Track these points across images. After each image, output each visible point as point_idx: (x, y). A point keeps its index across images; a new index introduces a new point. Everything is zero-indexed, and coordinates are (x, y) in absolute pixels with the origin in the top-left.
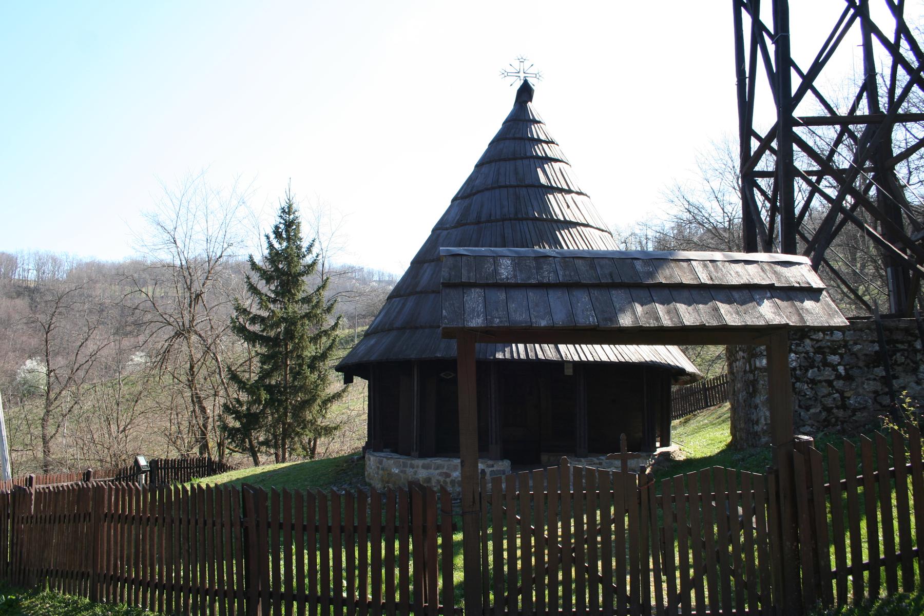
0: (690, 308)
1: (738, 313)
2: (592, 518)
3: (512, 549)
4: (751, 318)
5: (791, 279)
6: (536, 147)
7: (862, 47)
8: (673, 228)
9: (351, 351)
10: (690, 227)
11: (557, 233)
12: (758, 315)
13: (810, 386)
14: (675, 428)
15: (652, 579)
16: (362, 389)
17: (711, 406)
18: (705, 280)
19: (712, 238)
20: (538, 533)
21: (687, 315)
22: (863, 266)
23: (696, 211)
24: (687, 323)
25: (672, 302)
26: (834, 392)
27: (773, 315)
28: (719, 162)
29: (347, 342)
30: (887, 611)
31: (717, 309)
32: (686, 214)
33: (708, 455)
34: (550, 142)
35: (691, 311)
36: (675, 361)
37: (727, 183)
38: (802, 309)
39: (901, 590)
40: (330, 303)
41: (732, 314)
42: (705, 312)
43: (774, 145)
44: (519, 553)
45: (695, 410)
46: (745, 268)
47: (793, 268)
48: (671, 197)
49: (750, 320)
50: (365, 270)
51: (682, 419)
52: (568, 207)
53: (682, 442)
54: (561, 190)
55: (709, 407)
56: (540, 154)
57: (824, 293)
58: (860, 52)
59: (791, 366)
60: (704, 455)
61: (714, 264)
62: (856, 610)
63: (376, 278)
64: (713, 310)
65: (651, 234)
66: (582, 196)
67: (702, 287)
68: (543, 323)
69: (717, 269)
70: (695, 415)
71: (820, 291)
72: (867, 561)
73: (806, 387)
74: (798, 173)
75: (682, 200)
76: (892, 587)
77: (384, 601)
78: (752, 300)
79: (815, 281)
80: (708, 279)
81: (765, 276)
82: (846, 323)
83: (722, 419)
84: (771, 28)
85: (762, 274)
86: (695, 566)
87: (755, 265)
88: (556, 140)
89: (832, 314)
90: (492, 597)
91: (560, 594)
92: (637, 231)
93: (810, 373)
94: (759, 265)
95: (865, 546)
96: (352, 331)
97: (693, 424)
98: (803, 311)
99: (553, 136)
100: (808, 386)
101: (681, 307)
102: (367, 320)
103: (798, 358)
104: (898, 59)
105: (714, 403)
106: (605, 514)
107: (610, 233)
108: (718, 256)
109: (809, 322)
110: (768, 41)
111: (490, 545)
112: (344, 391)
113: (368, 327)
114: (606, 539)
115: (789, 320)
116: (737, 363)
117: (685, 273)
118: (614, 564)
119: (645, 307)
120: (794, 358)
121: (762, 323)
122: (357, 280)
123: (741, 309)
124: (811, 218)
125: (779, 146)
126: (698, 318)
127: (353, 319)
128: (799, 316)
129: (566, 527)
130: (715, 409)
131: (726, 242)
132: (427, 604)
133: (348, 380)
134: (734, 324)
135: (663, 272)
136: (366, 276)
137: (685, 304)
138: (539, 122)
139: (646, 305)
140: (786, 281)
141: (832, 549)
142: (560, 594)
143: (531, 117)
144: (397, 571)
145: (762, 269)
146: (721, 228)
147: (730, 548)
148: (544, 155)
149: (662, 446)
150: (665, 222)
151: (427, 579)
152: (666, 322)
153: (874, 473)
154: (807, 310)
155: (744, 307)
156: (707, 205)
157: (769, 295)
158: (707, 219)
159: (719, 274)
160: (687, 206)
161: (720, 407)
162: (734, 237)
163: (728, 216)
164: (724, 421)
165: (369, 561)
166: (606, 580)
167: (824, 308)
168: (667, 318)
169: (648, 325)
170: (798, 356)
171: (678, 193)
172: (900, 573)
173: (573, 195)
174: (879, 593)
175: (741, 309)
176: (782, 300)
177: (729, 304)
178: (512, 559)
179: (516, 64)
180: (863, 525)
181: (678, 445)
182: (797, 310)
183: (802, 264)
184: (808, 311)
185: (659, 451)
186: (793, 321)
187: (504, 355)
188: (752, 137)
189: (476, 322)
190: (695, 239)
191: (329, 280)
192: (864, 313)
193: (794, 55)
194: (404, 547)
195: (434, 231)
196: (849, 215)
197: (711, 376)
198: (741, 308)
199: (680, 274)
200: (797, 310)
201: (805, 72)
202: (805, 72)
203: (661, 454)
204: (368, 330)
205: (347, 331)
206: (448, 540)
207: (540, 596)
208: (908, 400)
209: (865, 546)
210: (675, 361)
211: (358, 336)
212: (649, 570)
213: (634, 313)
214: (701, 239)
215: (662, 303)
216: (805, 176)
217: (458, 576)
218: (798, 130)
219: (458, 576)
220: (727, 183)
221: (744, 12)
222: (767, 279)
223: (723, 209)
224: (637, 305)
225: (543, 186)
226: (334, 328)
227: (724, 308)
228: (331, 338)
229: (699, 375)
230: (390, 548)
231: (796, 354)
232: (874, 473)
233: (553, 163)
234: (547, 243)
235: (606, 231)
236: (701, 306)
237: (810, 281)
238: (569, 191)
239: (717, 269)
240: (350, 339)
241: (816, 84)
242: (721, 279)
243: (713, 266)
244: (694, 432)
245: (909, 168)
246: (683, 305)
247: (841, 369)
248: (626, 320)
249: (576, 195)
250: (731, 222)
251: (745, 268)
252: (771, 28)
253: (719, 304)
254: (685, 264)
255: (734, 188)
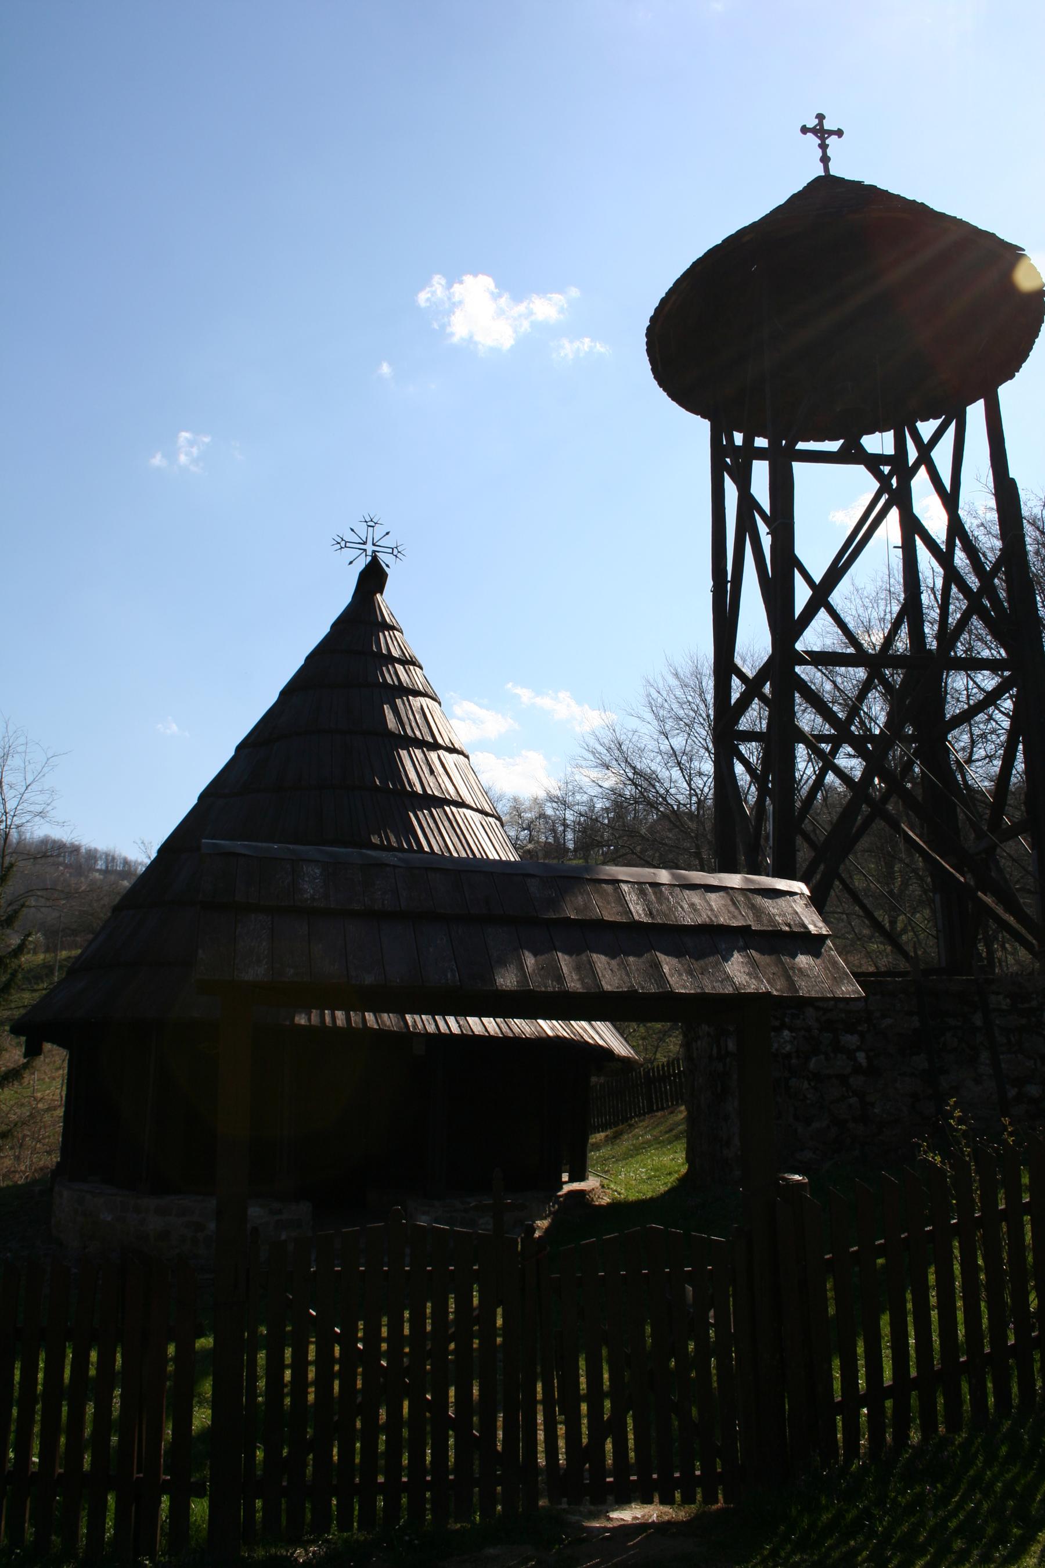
0: (614, 963)
1: (690, 973)
2: (440, 1310)
3: (300, 1364)
4: (712, 982)
5: (777, 918)
6: (384, 668)
7: (901, 550)
8: (607, 810)
9: (46, 996)
10: (635, 809)
11: (411, 815)
12: (723, 977)
13: (813, 1084)
14: (597, 1147)
15: (540, 1419)
16: (60, 1062)
17: (658, 1110)
18: (639, 915)
19: (670, 830)
20: (348, 1340)
21: (608, 974)
22: (905, 884)
23: (645, 784)
24: (607, 987)
25: (585, 951)
26: (851, 1094)
27: (747, 978)
28: (685, 706)
29: (38, 978)
30: (921, 1467)
31: (657, 966)
32: (629, 787)
33: (649, 1195)
34: (409, 662)
35: (615, 967)
36: (597, 1037)
37: (697, 742)
38: (793, 968)
39: (942, 1429)
40: (15, 907)
41: (680, 975)
42: (637, 970)
43: (767, 689)
44: (311, 1375)
45: (631, 1118)
46: (705, 899)
47: (782, 902)
48: (607, 758)
49: (710, 986)
50: (83, 850)
51: (609, 1132)
52: (432, 772)
53: (608, 1171)
54: (421, 744)
55: (654, 1111)
56: (389, 681)
57: (829, 942)
58: (897, 558)
59: (783, 1051)
60: (641, 1196)
61: (657, 890)
62: (873, 1467)
63: (100, 865)
64: (651, 966)
65: (570, 816)
66: (455, 755)
67: (635, 926)
68: (369, 980)
69: (660, 896)
70: (630, 1126)
71: (821, 938)
72: (891, 1383)
73: (806, 1085)
74: (800, 736)
75: (623, 765)
76: (928, 1427)
77: (61, 1471)
78: (714, 951)
79: (815, 924)
80: (646, 915)
81: (736, 913)
82: (858, 992)
83: (674, 1132)
84: (766, 506)
85: (732, 909)
86: (613, 1394)
87: (722, 894)
88: (421, 660)
89: (840, 977)
90: (260, 1454)
91: (382, 1448)
92: (549, 812)
93: (812, 1064)
94: (728, 893)
95: (886, 1353)
96: (49, 957)
97: (626, 1142)
98: (794, 972)
99: (415, 650)
100: (810, 1084)
101: (600, 960)
102: (78, 939)
103: (794, 1038)
104: (952, 576)
105: (662, 1105)
106: (463, 1302)
107: (499, 819)
108: (664, 876)
109: (802, 989)
110: (763, 528)
111: (262, 1356)
112: (25, 1066)
113: (79, 951)
114: (464, 1348)
115: (772, 986)
116: (699, 1043)
117: (608, 903)
118: (476, 1391)
119: (540, 958)
120: (788, 1039)
121: (729, 990)
122: (66, 866)
123: (696, 966)
124: (826, 805)
125: (772, 692)
126: (626, 978)
127: (54, 938)
128: (787, 980)
129: (395, 1327)
130: (664, 1116)
131: (692, 837)
132: (141, 1475)
133: (33, 1051)
134: (683, 991)
135: (573, 899)
136: (83, 860)
137: (606, 955)
138: (393, 628)
139: (542, 954)
140: (769, 922)
141: (836, 1363)
142: (382, 1448)
143: (380, 619)
144: (90, 1409)
145: (732, 900)
146: (685, 813)
147: (691, 1347)
148: (396, 683)
149: (572, 1180)
150: (595, 799)
151: (144, 1426)
152: (573, 983)
153: (903, 1236)
154: (800, 970)
155: (702, 962)
156: (663, 774)
157: (741, 943)
158: (663, 798)
159: (664, 907)
160: (630, 775)
161: (672, 1113)
162: (704, 829)
163: (696, 795)
164: (677, 1138)
165: (729, 578)
166: (461, 1426)
167: (826, 968)
168: (575, 977)
169: (543, 989)
170: (794, 1034)
171: (617, 753)
172: (941, 1400)
173: (441, 752)
174: (908, 1437)
175: (696, 966)
176: (762, 952)
177: (677, 957)
178: (300, 1382)
179: (362, 530)
180: (885, 1320)
181: (599, 1179)
182: (785, 971)
183: (795, 894)
184: (802, 972)
185: (566, 1188)
186: (778, 987)
187: (309, 1020)
188: (734, 677)
189: (256, 973)
190: (643, 831)
191: (15, 869)
192: (903, 965)
193: (802, 550)
194: (107, 1359)
195: (203, 797)
196: (878, 809)
197: (662, 1059)
198: (696, 965)
199: (600, 904)
200: (785, 971)
201: (817, 579)
202: (817, 579)
203: (571, 1193)
204: (81, 954)
205: (41, 956)
206: (186, 1349)
207: (347, 1453)
208: (957, 1113)
209: (886, 1353)
210: (597, 1037)
211: (61, 967)
212: (535, 1402)
213: (521, 967)
214: (651, 829)
215: (568, 952)
216: (812, 742)
217: (202, 1417)
218: (803, 671)
219: (202, 1417)
220: (697, 742)
221: (728, 481)
222: (740, 917)
223: (689, 785)
224: (527, 953)
225: (391, 734)
226: (20, 949)
227: (668, 965)
228: (9, 971)
229: (636, 1061)
230: (81, 1363)
231: (791, 1031)
232: (903, 1236)
233: (411, 698)
234: (392, 831)
235: (492, 816)
236: (631, 959)
237: (806, 922)
238: (435, 746)
239: (660, 896)
240: (48, 969)
241: (836, 598)
242: (665, 915)
243: (655, 893)
244: (628, 1156)
245: (972, 735)
246: (603, 958)
247: (861, 1056)
248: (507, 980)
249: (446, 754)
250: (701, 805)
251: (705, 899)
252: (766, 506)
253: (662, 957)
254: (609, 888)
255: (707, 749)
